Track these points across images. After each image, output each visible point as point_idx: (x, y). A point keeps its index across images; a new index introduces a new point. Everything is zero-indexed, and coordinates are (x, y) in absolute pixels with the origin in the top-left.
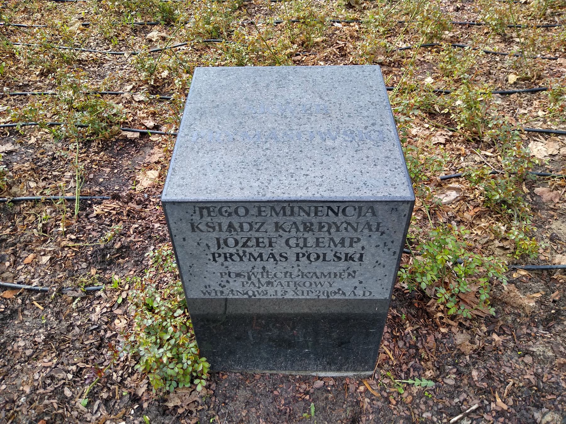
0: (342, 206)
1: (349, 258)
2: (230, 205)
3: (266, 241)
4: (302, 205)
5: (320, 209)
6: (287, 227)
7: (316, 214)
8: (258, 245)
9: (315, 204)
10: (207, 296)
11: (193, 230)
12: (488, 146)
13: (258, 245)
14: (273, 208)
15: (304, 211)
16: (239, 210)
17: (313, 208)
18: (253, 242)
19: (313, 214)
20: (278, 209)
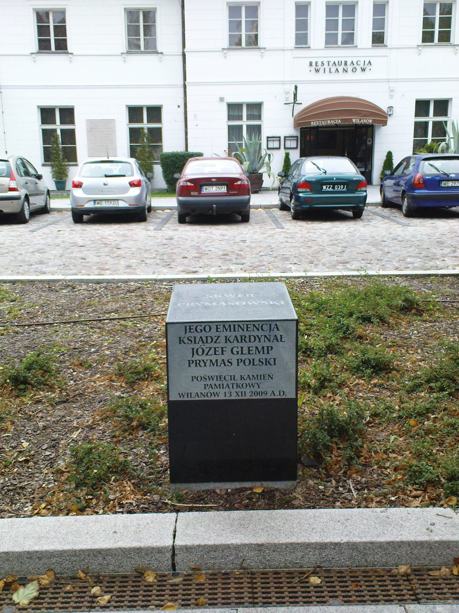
0: (195, 325)
1: (267, 362)
2: (201, 324)
3: (254, 349)
4: (256, 324)
5: (249, 326)
6: (231, 339)
7: (247, 330)
8: (215, 354)
9: (217, 324)
10: (182, 399)
11: (180, 343)
12: (68, 286)
13: (215, 354)
14: (224, 326)
15: (241, 327)
16: (264, 326)
17: (245, 326)
18: (212, 351)
19: (245, 330)
20: (227, 327)
